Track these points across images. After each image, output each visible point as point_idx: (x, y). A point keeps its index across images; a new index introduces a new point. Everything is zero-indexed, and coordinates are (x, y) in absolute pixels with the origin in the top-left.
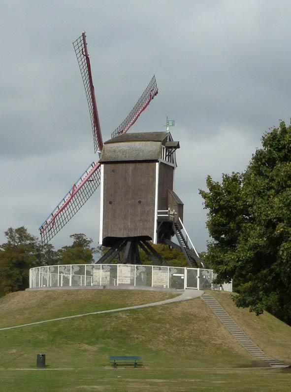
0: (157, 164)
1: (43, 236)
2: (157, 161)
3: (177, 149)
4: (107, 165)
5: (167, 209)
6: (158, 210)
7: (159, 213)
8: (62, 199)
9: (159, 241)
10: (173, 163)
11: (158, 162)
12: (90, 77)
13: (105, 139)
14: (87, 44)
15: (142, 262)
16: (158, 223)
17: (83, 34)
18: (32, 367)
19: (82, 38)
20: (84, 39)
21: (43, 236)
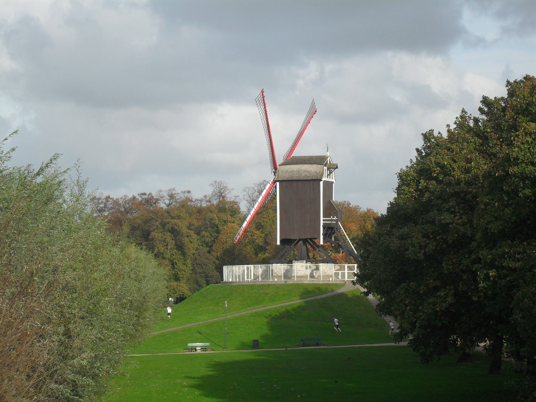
5: (331, 218)
7: (324, 220)
14: (266, 104)
16: (324, 228)
17: (262, 92)
19: (261, 94)
21: (315, 108)
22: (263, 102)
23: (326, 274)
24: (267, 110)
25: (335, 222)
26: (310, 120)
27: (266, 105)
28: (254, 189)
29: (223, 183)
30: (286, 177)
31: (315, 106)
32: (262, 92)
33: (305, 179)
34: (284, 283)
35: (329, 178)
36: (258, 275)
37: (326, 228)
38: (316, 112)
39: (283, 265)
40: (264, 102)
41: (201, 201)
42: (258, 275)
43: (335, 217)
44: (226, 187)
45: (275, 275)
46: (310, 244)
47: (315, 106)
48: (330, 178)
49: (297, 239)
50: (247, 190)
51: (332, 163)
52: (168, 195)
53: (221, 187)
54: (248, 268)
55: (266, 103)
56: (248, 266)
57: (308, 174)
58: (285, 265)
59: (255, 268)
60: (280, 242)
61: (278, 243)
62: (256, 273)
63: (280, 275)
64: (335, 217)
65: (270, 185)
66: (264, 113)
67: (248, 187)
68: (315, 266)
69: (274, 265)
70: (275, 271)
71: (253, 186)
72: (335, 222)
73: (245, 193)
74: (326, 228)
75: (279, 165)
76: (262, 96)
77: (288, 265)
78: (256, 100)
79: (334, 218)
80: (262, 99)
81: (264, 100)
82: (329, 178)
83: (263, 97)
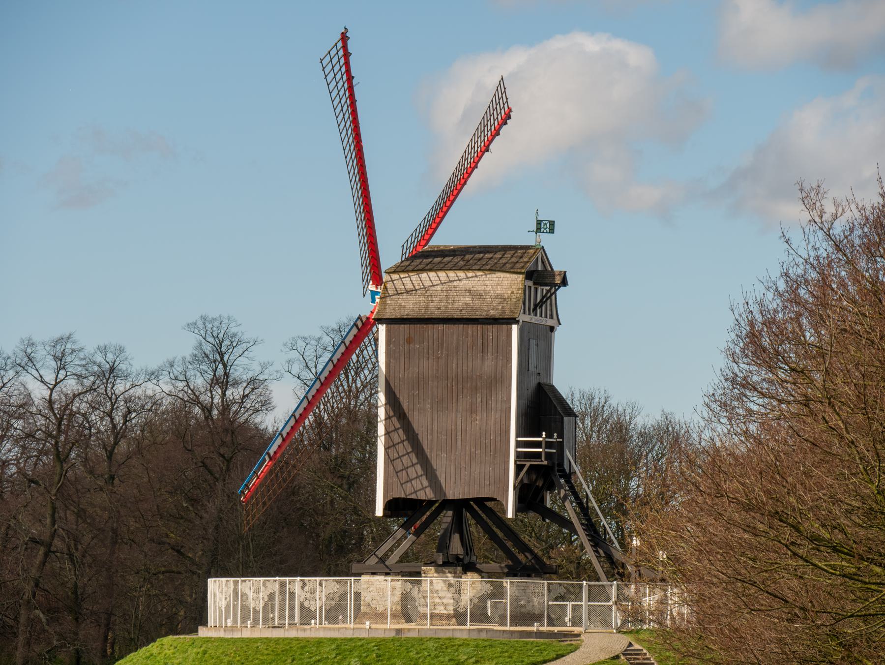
0: (515, 328)
1: (506, 106)
2: (514, 321)
3: (562, 288)
4: (392, 326)
5: (540, 436)
6: (518, 436)
7: (519, 444)
8: (334, 44)
9: (518, 509)
10: (552, 317)
11: (517, 322)
12: (354, 113)
13: (390, 257)
14: (353, 77)
15: (555, 622)
16: (519, 468)
17: (344, 38)
18: (241, 591)
19: (340, 45)
20: (345, 47)
21: (506, 106)
22: (344, 69)
23: (523, 610)
24: (357, 96)
25: (555, 451)
26: (490, 141)
27: (354, 82)
28: (322, 342)
29: (226, 321)
30: (410, 306)
31: (507, 99)
32: (344, 38)
33: (466, 316)
34: (392, 634)
35: (541, 316)
36: (313, 610)
37: (525, 469)
38: (509, 118)
39: (389, 578)
40: (348, 72)
41: (153, 376)
42: (313, 610)
43: (555, 435)
44: (234, 335)
45: (368, 610)
46: (475, 515)
47: (507, 99)
48: (543, 315)
49: (436, 501)
50: (301, 344)
51: (550, 270)
52: (752, 324)
53: (221, 336)
54: (282, 585)
55: (353, 75)
56: (542, 287)
57: (477, 304)
58: (398, 580)
59: (306, 588)
60: (385, 509)
61: (379, 512)
62: (306, 604)
63: (380, 609)
64: (555, 435)
65: (357, 330)
66: (346, 105)
67: (305, 338)
68: (489, 585)
69: (364, 578)
70: (366, 597)
71: (318, 333)
72: (555, 451)
73: (294, 355)
74: (525, 469)
75: (388, 273)
76: (341, 53)
77: (406, 581)
78: (325, 62)
79: (552, 437)
80: (342, 61)
81: (347, 64)
82: (541, 316)
83: (347, 55)
